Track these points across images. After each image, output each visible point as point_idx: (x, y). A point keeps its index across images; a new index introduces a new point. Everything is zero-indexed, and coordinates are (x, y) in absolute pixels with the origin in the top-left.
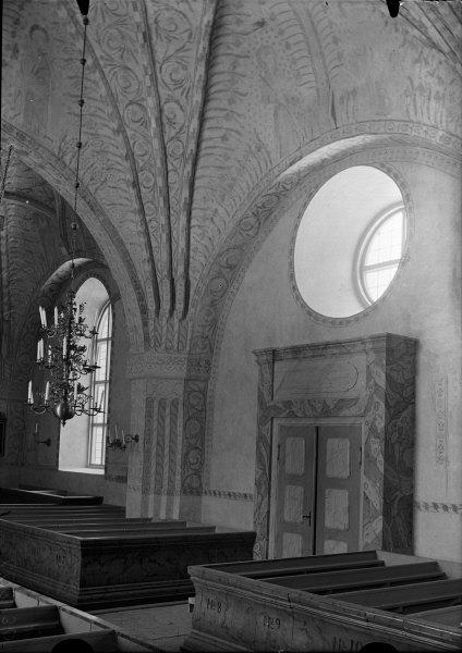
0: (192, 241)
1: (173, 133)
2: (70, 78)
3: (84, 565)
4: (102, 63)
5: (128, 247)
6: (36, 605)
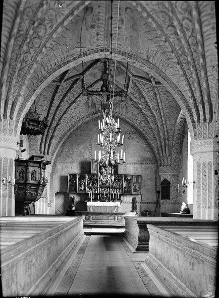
0: (210, 83)
1: (190, 34)
2: (144, 24)
3: (140, 233)
4: (151, 13)
5: (183, 93)
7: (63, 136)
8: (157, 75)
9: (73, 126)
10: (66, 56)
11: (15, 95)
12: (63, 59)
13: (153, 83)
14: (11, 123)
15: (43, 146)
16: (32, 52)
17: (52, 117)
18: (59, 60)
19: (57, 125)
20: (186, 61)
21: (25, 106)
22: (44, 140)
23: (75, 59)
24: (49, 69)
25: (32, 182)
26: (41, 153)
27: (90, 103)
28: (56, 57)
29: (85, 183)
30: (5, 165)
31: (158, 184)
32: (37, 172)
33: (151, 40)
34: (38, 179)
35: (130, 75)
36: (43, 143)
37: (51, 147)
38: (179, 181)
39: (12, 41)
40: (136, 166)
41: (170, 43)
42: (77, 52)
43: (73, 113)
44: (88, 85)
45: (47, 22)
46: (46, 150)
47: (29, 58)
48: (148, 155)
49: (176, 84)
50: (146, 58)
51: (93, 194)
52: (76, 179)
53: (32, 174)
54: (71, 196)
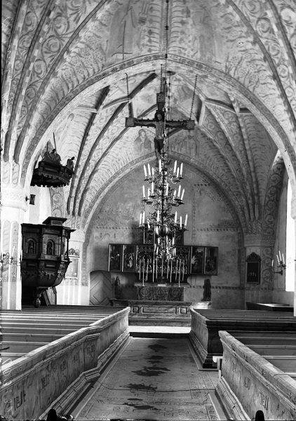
2: (222, 17)
5: (281, 123)
6: (212, 285)
7: (103, 189)
8: (241, 95)
9: (118, 173)
10: (100, 65)
11: (21, 125)
12: (96, 71)
13: (237, 110)
14: (16, 169)
15: (72, 203)
16: (47, 57)
17: (85, 161)
18: (91, 71)
19: (93, 173)
20: (286, 73)
21: (37, 143)
22: (73, 195)
23: (114, 70)
24: (75, 86)
25: (47, 257)
26: (69, 213)
27: (143, 140)
28: (85, 67)
29: (134, 258)
30: (5, 233)
31: (242, 260)
32: (57, 242)
33: (231, 41)
34: (58, 253)
35: (202, 99)
36: (72, 199)
37: (84, 205)
38: (272, 256)
39: (16, 41)
40: (210, 233)
41: (262, 46)
42: (118, 60)
43: (117, 155)
44: (140, 113)
45: (70, 12)
46: (77, 209)
47: (43, 69)
48: (229, 217)
49: (270, 110)
50: (224, 69)
51: (145, 274)
52: (120, 252)
53: (48, 246)
54: (114, 276)
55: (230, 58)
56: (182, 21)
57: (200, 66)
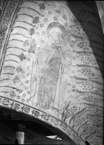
55: (70, 107)
56: (23, 54)
57: (40, 96)
